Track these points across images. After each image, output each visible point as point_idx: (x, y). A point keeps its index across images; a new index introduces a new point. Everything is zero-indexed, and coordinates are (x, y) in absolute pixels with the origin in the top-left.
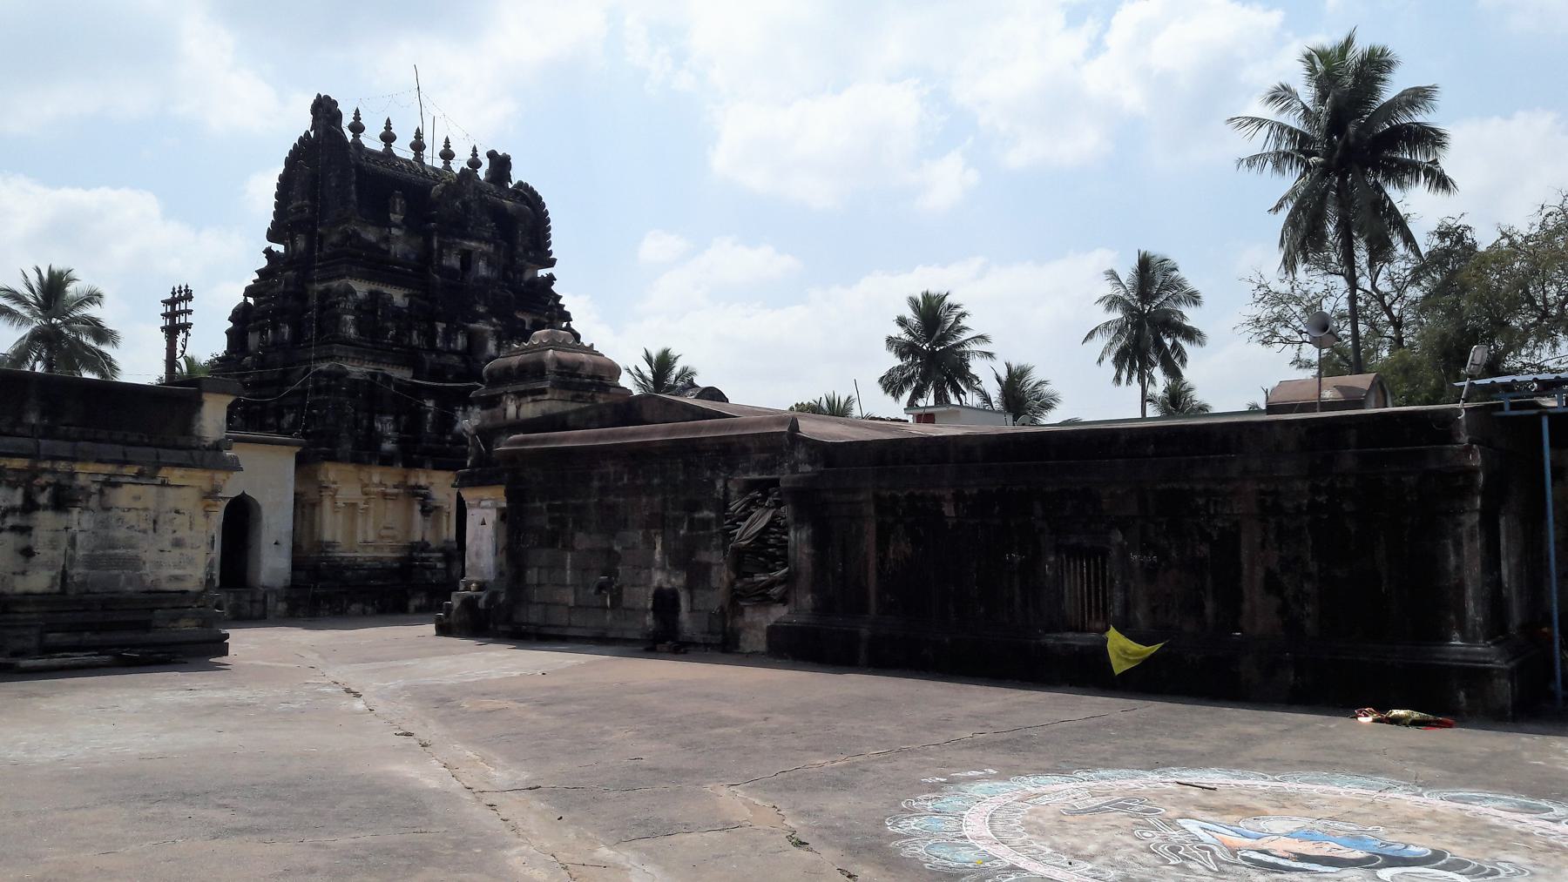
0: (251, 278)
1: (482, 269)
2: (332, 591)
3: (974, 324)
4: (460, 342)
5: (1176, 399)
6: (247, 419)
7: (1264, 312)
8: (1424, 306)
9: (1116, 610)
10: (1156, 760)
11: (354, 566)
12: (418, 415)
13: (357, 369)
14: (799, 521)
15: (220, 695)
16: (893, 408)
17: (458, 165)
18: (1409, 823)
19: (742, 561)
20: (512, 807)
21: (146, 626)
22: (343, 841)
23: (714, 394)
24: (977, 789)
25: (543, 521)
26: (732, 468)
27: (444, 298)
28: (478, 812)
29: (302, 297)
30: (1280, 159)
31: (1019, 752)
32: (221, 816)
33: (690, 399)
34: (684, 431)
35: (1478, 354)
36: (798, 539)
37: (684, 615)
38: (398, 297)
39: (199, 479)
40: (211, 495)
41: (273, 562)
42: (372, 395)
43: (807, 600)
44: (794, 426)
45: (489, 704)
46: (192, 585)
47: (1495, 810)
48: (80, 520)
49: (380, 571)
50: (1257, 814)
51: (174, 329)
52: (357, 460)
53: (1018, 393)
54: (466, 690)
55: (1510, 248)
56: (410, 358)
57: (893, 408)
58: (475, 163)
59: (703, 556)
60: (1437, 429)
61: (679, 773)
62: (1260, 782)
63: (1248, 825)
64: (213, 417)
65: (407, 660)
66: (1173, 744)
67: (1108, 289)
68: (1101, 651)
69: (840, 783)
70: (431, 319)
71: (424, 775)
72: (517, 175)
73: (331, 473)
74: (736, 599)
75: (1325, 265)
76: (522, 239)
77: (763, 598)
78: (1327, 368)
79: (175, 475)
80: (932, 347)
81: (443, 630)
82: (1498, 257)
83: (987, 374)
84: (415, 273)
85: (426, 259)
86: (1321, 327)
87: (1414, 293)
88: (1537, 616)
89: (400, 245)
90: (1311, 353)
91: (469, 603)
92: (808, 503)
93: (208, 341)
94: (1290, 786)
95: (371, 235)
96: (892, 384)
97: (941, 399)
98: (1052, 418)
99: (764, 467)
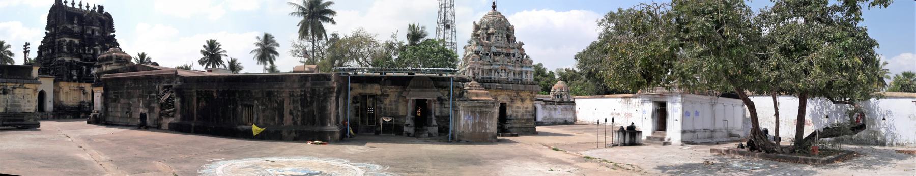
0: (42, 39)
1: (97, 33)
2: (62, 113)
3: (223, 48)
4: (92, 52)
5: (273, 69)
6: (43, 72)
7: (294, 49)
8: (328, 50)
9: (255, 120)
10: (261, 156)
11: (68, 107)
12: (82, 70)
13: (67, 59)
14: (177, 96)
15: (38, 136)
16: (202, 68)
17: (90, 9)
18: (316, 166)
19: (162, 106)
20: (106, 165)
21: (23, 120)
22: (67, 171)
23: (156, 64)
24: (220, 163)
25: (112, 96)
26: (160, 83)
27: (88, 41)
28: (97, 166)
29: (54, 42)
30: (299, 14)
31: (230, 154)
32: (40, 163)
33: (149, 65)
34: (148, 73)
35: (337, 62)
36: (177, 101)
37: (148, 119)
38: (77, 41)
39: (32, 86)
40: (35, 90)
41: (49, 106)
42: (71, 65)
43: (179, 116)
44: (176, 72)
45: (100, 140)
46: (32, 111)
47: (334, 162)
48: (8, 96)
49: (74, 108)
50: (283, 166)
51: (26, 52)
52: (67, 81)
53: (233, 65)
54: (94, 137)
55: (346, 39)
56: (80, 56)
57: (202, 68)
58: (95, 8)
59: (153, 105)
60: (327, 78)
61: (146, 159)
62: (284, 159)
63: (281, 169)
64: (35, 72)
65: (80, 129)
66: (266, 151)
67: (257, 41)
68: (251, 130)
69: (186, 162)
70: (84, 46)
71: (85, 157)
72: (105, 10)
73: (62, 84)
74: (161, 115)
75: (308, 39)
76: (107, 25)
77: (168, 116)
78: (307, 63)
79: (27, 86)
80: (212, 53)
81: (89, 122)
82: (344, 41)
83: (226, 60)
84: (80, 35)
85: (83, 32)
86: (306, 54)
87: (326, 47)
88: (344, 122)
89: (77, 29)
90: (303, 59)
91: (95, 116)
92: (179, 92)
93: (33, 55)
94: (291, 160)
95: (69, 27)
96: (202, 62)
97: (214, 66)
98: (242, 72)
99: (168, 83)
